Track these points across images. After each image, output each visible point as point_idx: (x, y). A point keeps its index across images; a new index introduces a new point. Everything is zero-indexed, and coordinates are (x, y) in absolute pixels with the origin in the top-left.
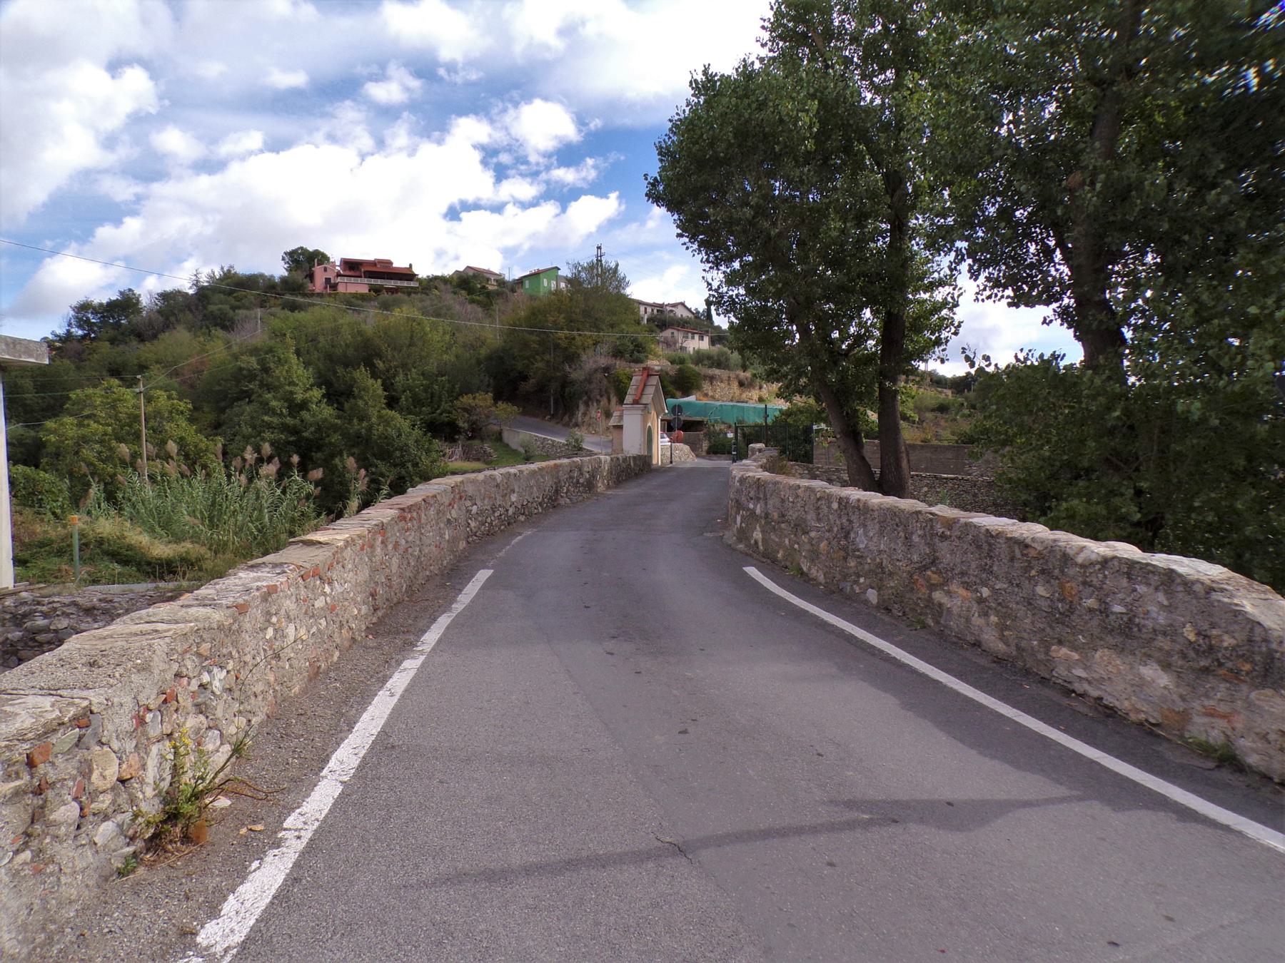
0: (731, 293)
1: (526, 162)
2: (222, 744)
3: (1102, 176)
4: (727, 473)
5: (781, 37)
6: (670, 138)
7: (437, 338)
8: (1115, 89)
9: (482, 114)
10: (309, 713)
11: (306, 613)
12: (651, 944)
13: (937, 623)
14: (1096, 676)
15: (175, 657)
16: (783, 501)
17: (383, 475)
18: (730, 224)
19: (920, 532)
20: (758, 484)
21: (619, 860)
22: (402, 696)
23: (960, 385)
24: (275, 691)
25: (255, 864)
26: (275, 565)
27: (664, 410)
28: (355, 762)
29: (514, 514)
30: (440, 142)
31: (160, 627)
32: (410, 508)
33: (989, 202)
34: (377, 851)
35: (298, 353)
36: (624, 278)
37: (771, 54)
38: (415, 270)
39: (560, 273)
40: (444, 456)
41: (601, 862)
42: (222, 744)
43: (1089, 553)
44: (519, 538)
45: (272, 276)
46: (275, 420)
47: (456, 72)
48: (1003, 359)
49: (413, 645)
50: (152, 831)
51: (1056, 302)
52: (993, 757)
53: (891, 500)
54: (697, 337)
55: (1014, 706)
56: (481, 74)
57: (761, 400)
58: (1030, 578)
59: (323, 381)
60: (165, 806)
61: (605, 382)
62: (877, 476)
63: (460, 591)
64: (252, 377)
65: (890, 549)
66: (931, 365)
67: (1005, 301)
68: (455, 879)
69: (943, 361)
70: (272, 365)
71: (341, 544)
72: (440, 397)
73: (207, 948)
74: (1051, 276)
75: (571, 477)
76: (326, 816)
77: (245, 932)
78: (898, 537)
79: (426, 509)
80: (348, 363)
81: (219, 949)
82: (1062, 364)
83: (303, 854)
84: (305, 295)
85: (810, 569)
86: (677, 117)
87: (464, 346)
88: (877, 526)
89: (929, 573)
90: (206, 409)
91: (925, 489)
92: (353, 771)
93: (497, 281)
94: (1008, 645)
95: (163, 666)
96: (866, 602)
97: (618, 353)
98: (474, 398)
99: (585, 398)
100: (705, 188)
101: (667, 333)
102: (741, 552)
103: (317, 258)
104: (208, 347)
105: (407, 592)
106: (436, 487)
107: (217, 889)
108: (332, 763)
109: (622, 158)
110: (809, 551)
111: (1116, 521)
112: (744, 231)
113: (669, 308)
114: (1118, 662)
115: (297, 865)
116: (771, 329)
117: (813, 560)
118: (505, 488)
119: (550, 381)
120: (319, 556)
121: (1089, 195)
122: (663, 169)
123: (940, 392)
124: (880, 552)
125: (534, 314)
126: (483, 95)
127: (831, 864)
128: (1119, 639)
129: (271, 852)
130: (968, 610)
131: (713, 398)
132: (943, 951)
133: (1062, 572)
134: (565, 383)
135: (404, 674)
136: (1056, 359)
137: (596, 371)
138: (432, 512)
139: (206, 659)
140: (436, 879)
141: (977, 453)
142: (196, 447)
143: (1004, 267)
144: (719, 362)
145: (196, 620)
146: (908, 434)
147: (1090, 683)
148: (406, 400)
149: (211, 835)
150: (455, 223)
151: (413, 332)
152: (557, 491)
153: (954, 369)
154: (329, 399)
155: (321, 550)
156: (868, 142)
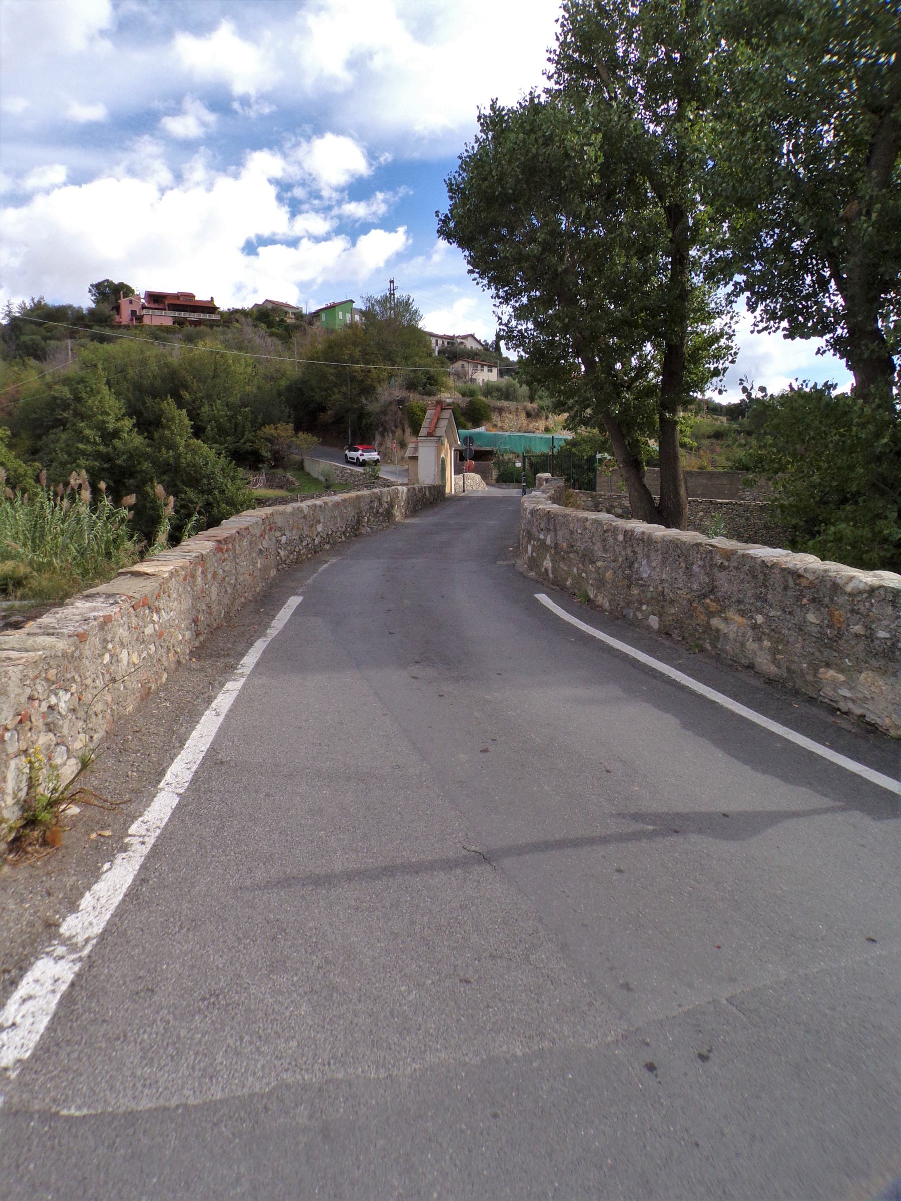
0: (519, 327)
1: (320, 197)
2: (68, 758)
3: (878, 206)
4: (517, 502)
5: (567, 70)
6: (460, 175)
7: (240, 369)
8: (893, 115)
9: (276, 148)
10: (143, 730)
11: (137, 639)
12: (460, 941)
13: (714, 646)
14: (860, 695)
15: (27, 682)
16: (572, 533)
17: (192, 502)
18: (519, 259)
19: (700, 563)
20: (549, 517)
21: (430, 867)
22: (227, 716)
23: (734, 412)
24: (112, 710)
25: (106, 866)
26: (108, 596)
27: (456, 442)
28: (188, 776)
29: (320, 543)
30: (236, 176)
31: (13, 654)
32: (226, 541)
33: (767, 234)
34: (213, 856)
35: (108, 383)
36: (416, 311)
37: (557, 87)
38: (217, 303)
39: (354, 305)
40: (248, 484)
41: (415, 869)
42: (68, 758)
43: (858, 583)
44: (326, 566)
45: (80, 308)
46: (89, 448)
47: (250, 106)
48: (777, 387)
49: (233, 667)
50: (13, 835)
51: (829, 332)
52: (765, 772)
53: (673, 533)
54: (485, 369)
55: (784, 724)
56: (274, 107)
57: (547, 430)
58: (802, 606)
59: (133, 411)
60: (23, 812)
61: (400, 414)
62: (657, 503)
63: (274, 616)
64: (65, 406)
65: (672, 578)
66: (711, 394)
67: (780, 333)
68: (286, 882)
69: (720, 392)
70: (84, 395)
71: (166, 575)
72: (244, 427)
73: (70, 938)
74: (826, 307)
75: (372, 508)
76: (167, 824)
77: (102, 925)
78: (679, 568)
79: (240, 541)
80: (156, 394)
81: (80, 939)
82: (834, 393)
83: (148, 858)
84: (112, 327)
85: (596, 596)
86: (466, 154)
87: (265, 377)
88: (660, 558)
89: (708, 601)
90: (23, 436)
91: (701, 514)
92: (187, 784)
93: (295, 314)
94: (779, 666)
95: (17, 690)
96: (648, 628)
97: (411, 386)
98: (276, 429)
99: (381, 429)
100: (495, 224)
101: (458, 365)
102: (532, 580)
103: (121, 290)
104: (22, 376)
105: (225, 617)
106: (248, 519)
107: (73, 887)
108: (168, 776)
109: (411, 192)
110: (595, 579)
111: (880, 543)
112: (533, 268)
113: (459, 340)
114: (881, 683)
115: (143, 867)
116: (558, 363)
117: (599, 588)
118: (312, 519)
119: (347, 412)
120: (145, 587)
121: (866, 225)
122: (454, 206)
123: (716, 420)
124: (662, 581)
125: (330, 347)
126: (275, 128)
127: (619, 871)
128: (883, 662)
129: (120, 856)
130: (744, 635)
131: (502, 428)
132: (719, 947)
133: (832, 600)
134: (362, 414)
135: (227, 695)
136: (829, 389)
137: (391, 403)
138: (245, 543)
139: (53, 684)
140: (268, 882)
141: (751, 481)
142: (15, 471)
143: (781, 300)
144: (506, 394)
145: (43, 648)
146: (686, 462)
147: (854, 701)
149: (66, 838)
150: (252, 257)
151: (216, 364)
152: (359, 522)
153: (733, 397)
154: (139, 428)
155: (149, 581)
156: (652, 177)
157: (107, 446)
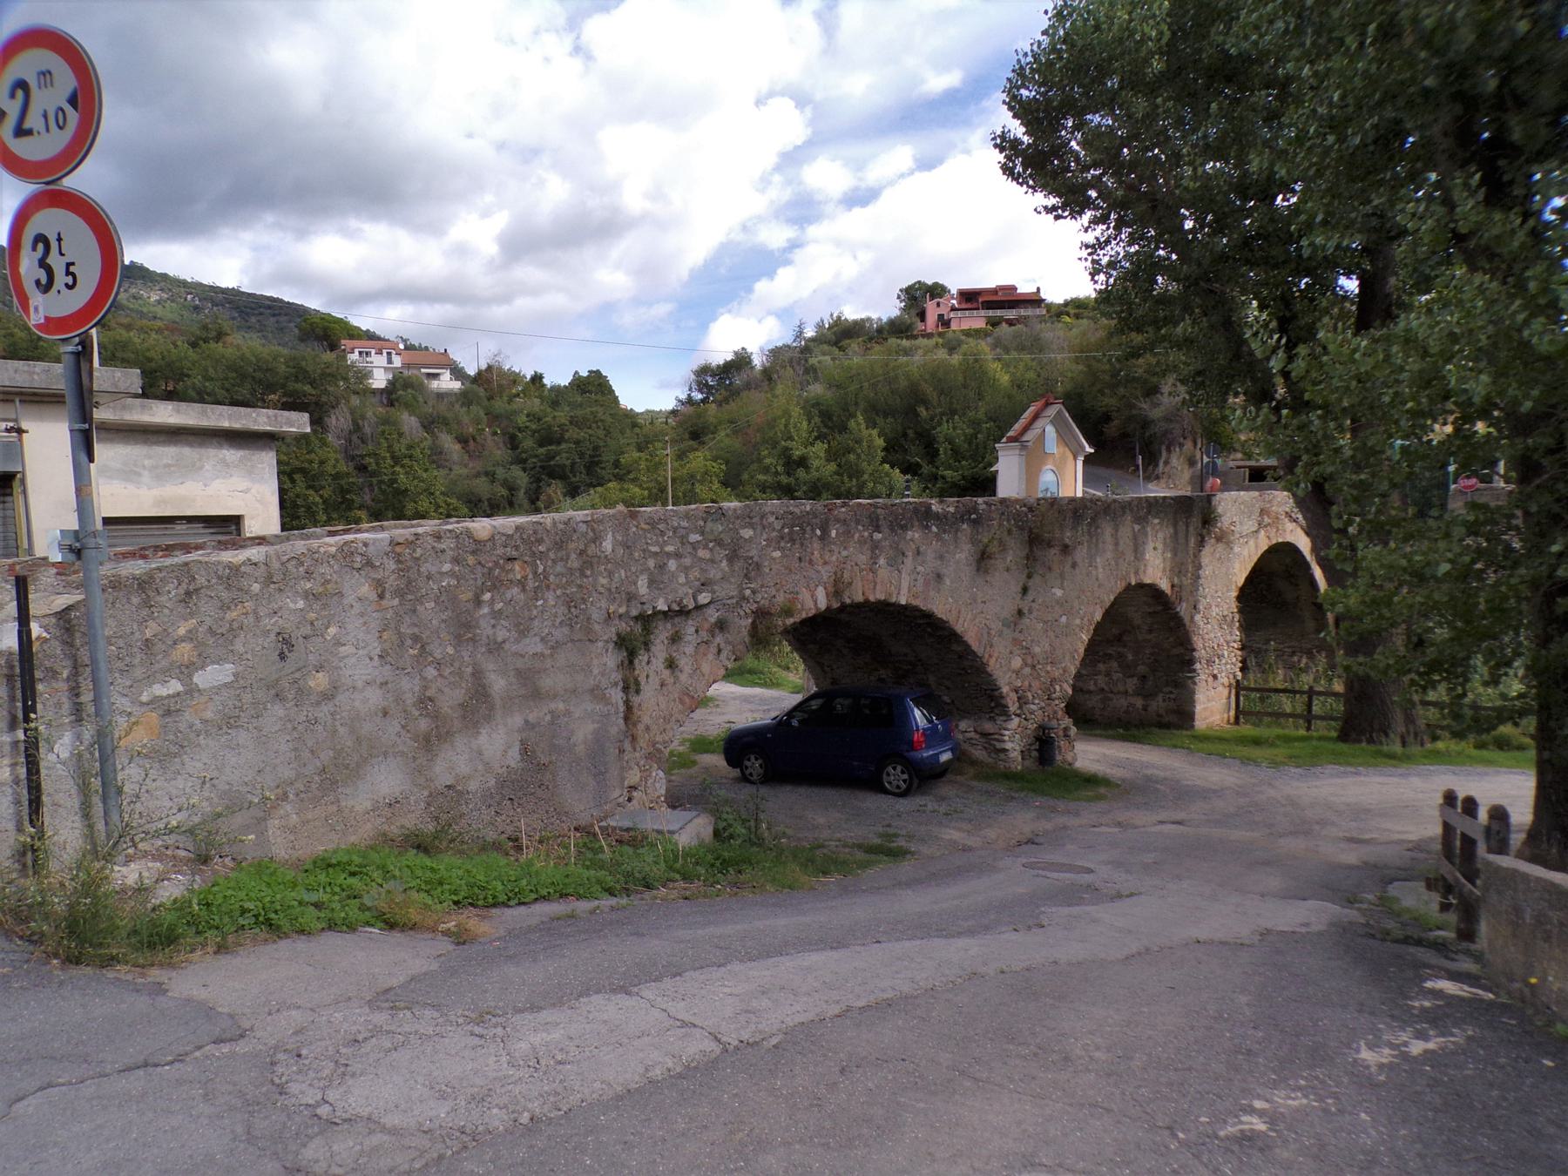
27: (1083, 448)
38: (1043, 295)
103: (937, 291)
148: (945, 453)
157: (789, 474)
